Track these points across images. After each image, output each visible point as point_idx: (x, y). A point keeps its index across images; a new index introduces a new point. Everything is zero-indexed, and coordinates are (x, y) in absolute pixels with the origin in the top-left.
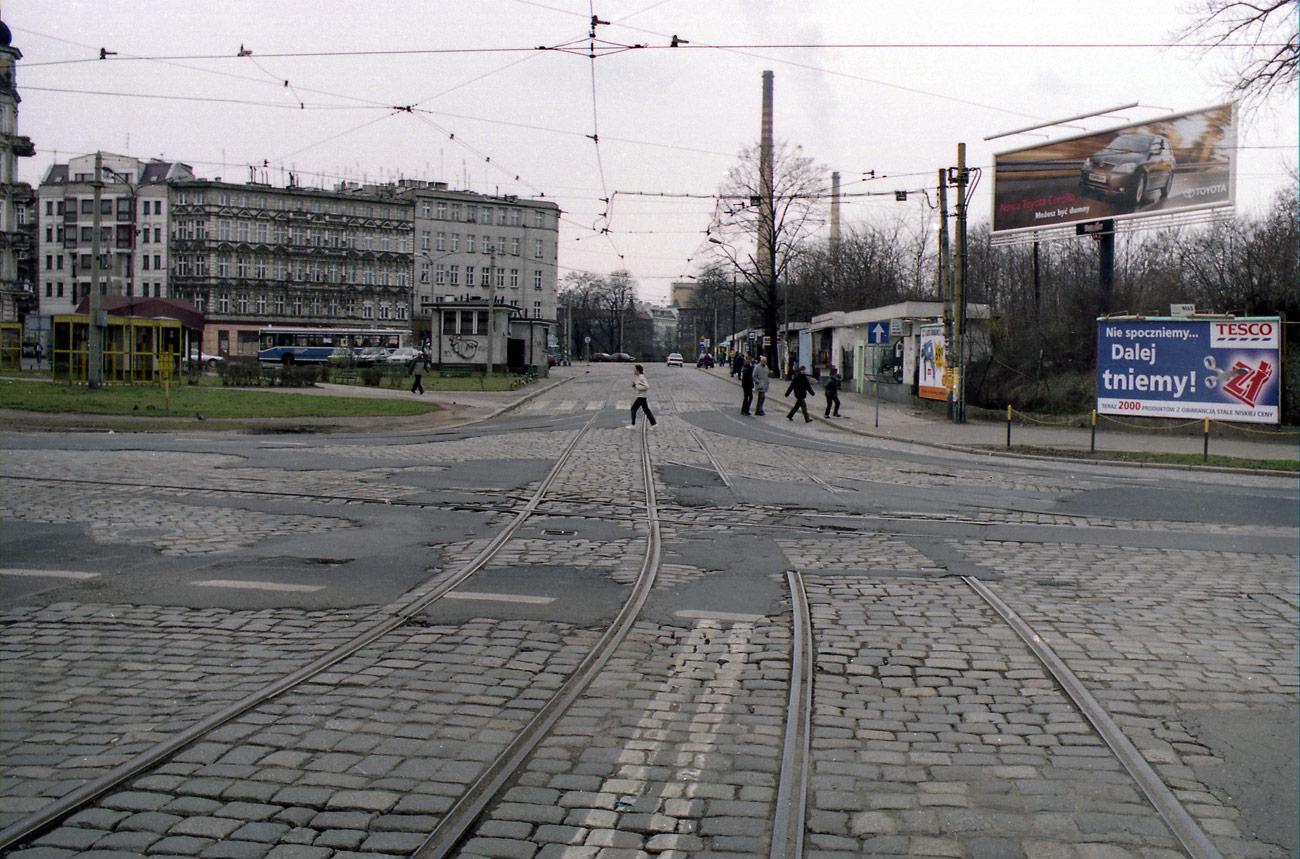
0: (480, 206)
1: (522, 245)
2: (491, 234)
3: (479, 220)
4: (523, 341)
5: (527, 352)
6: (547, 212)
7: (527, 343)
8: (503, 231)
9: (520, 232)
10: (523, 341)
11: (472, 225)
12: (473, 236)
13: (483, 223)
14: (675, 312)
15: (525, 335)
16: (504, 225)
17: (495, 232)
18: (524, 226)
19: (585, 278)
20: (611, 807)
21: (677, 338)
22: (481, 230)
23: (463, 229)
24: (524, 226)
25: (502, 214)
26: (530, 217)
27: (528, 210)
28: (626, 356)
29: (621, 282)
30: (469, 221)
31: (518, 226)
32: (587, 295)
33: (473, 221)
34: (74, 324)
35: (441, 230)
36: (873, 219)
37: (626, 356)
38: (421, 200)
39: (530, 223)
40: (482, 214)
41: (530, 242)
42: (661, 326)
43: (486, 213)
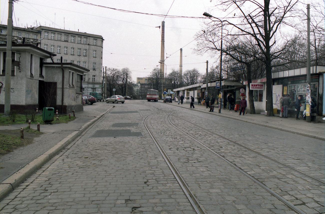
0: (70, 35)
1: (88, 52)
2: (75, 47)
3: (69, 41)
4: (55, 84)
5: (59, 92)
6: (98, 39)
7: (59, 86)
8: (80, 46)
9: (87, 47)
10: (55, 84)
11: (66, 43)
12: (67, 47)
13: (71, 42)
14: (139, 85)
15: (57, 78)
16: (81, 43)
17: (76, 46)
18: (89, 44)
19: (113, 70)
20: (125, 203)
21: (140, 92)
22: (70, 45)
23: (63, 44)
24: (89, 44)
25: (79, 39)
26: (91, 41)
27: (90, 38)
28: (128, 97)
29: (126, 73)
30: (65, 41)
31: (86, 44)
32: (114, 76)
33: (67, 41)
34: (258, 101)
35: (52, 44)
36: (5, 191)
37: (128, 97)
38: (44, 31)
39: (91, 43)
40: (71, 39)
41: (91, 51)
42: (136, 89)
43: (73, 38)
